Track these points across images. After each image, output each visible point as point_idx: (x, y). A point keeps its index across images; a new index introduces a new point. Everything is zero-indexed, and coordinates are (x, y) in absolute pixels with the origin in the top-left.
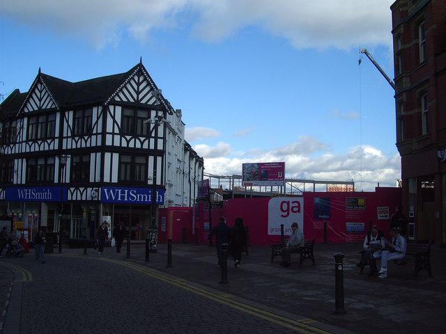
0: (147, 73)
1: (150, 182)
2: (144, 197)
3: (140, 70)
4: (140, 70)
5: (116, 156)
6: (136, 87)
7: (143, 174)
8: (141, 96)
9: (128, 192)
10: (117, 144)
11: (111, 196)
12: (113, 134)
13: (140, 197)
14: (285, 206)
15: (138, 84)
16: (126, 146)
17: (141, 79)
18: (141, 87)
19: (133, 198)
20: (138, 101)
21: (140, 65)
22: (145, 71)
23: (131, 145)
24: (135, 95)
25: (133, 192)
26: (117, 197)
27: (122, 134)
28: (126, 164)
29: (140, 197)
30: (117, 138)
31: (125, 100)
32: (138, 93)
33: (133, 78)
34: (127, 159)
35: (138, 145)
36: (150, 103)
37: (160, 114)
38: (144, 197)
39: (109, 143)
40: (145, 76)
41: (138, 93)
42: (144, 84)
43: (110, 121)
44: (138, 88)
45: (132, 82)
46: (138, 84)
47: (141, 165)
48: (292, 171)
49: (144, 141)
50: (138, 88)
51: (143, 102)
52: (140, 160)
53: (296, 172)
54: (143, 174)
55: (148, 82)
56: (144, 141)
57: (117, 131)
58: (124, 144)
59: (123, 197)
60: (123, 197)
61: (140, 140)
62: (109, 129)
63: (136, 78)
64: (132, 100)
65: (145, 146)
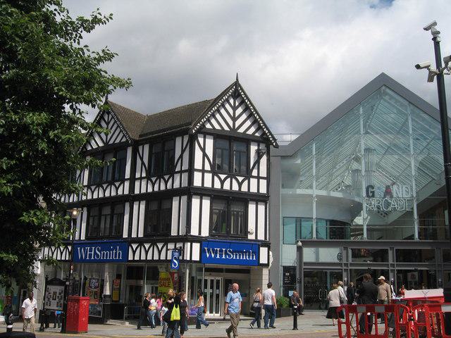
1: (125, 235)
3: (236, 90)
8: (238, 123)
10: (208, 184)
12: (203, 171)
15: (235, 108)
20: (234, 130)
22: (243, 91)
23: (227, 186)
24: (231, 123)
31: (217, 127)
35: (235, 187)
36: (118, 141)
41: (234, 119)
43: (198, 154)
44: (234, 113)
45: (227, 106)
46: (235, 108)
50: (234, 113)
52: (236, 208)
58: (217, 185)
62: (198, 164)
63: (232, 101)
64: (226, 128)
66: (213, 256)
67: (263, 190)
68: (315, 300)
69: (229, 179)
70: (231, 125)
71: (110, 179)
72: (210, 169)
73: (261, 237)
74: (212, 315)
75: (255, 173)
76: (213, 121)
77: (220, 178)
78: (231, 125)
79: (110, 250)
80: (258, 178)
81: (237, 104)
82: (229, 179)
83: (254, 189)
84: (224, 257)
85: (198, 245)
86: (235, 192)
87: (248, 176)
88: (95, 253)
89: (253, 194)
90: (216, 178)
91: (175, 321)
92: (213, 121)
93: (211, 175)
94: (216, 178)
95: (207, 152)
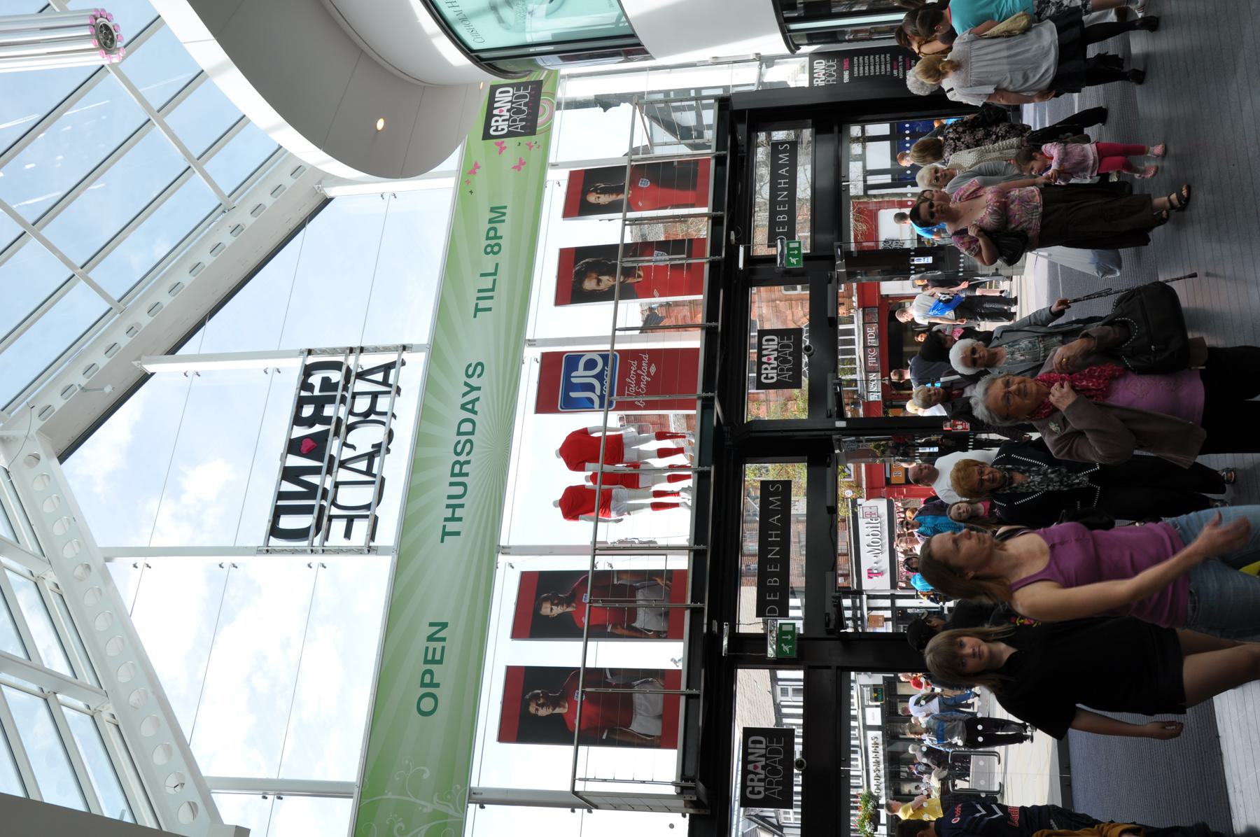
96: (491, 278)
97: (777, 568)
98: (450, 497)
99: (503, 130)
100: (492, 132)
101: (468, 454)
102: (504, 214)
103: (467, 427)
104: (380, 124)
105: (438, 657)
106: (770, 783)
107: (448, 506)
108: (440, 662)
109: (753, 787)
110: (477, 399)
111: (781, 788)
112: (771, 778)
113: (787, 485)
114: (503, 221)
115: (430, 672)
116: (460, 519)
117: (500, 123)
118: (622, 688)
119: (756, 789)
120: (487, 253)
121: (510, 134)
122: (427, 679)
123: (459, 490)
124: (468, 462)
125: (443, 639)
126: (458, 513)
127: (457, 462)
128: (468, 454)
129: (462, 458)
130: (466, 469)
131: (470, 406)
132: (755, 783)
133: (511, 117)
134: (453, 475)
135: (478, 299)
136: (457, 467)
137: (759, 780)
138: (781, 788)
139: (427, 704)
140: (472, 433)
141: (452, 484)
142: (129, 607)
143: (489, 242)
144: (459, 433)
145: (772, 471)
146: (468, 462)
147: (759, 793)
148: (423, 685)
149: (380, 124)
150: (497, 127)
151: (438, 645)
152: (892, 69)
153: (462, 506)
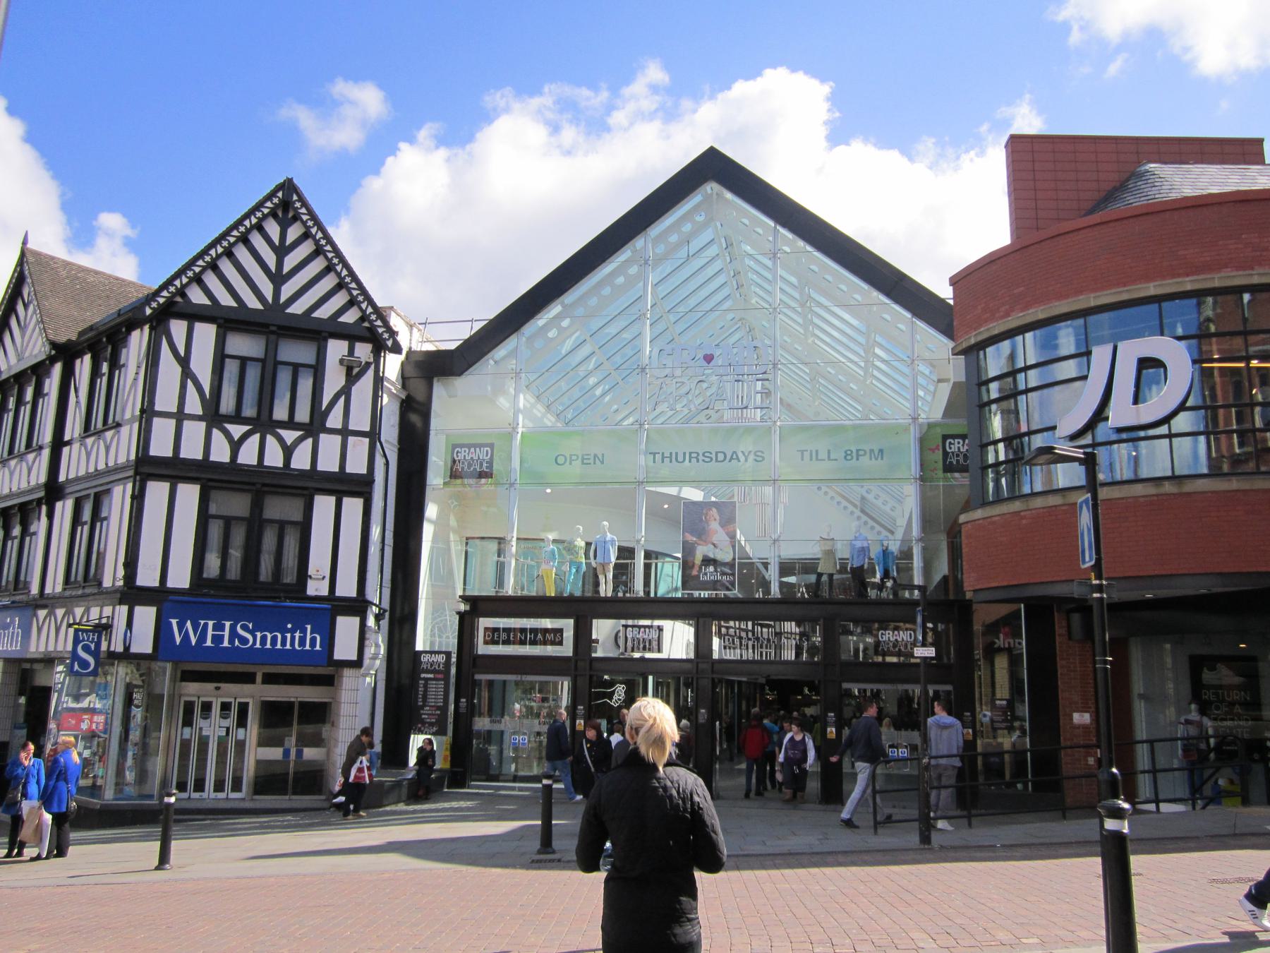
0: (311, 213)
1: (317, 587)
2: (274, 640)
3: (286, 205)
4: (286, 205)
5: (189, 494)
6: (270, 259)
7: (290, 559)
8: (287, 290)
9: (233, 628)
10: (192, 450)
11: (186, 637)
12: (180, 416)
13: (264, 639)
14: (849, 452)
15: (282, 251)
16: (279, 463)
17: (294, 232)
18: (290, 262)
19: (244, 641)
20: (276, 307)
21: (288, 187)
22: (305, 204)
23: (248, 456)
24: (267, 288)
25: (245, 628)
26: (202, 638)
27: (213, 417)
28: (228, 522)
29: (264, 639)
30: (194, 433)
31: (226, 300)
32: (278, 279)
33: (259, 228)
34: (236, 504)
35: (274, 458)
36: (324, 312)
37: (363, 351)
38: (274, 640)
39: (161, 447)
40: (317, 242)
41: (278, 279)
42: (306, 249)
43: (169, 370)
44: (280, 264)
45: (257, 240)
46: (282, 251)
47: (282, 525)
48: (1199, 427)
49: (245, 437)
50: (280, 264)
51: (298, 308)
52: (280, 508)
53: (41, 816)
54: (290, 559)
55: (317, 242)
56: (245, 437)
57: (194, 405)
58: (221, 453)
59: (218, 639)
60: (218, 639)
61: (281, 440)
62: (166, 399)
63: (273, 229)
64: (253, 303)
65: (301, 460)
66: (194, 641)
67: (357, 465)
68: (858, 715)
69: (257, 437)
70: (269, 294)
71: (303, 415)
72: (201, 413)
73: (347, 588)
74: (221, 795)
75: (334, 420)
76: (211, 280)
77: (281, 440)
78: (269, 294)
79: (284, 631)
80: (345, 432)
81: (290, 240)
82: (257, 437)
83: (329, 463)
84: (226, 644)
85: (152, 611)
86: (272, 471)
87: (315, 427)
88: (234, 633)
89: (328, 476)
90: (216, 433)
91: (1087, 761)
92: (211, 280)
93: (202, 426)
94: (216, 433)
95: (194, 366)
96: (826, 456)
97: (559, 631)
98: (677, 454)
99: (950, 448)
100: (948, 441)
101: (703, 460)
102: (876, 459)
103: (721, 457)
104: (666, 506)
105: (585, 461)
106: (958, 456)
107: (671, 454)
108: (583, 463)
109: (953, 444)
110: (739, 461)
111: (955, 463)
112: (961, 456)
113: (560, 643)
114: (871, 459)
115: (577, 459)
116: (663, 462)
117: (957, 445)
118: (290, 705)
119: (952, 446)
120: (846, 452)
121: (945, 454)
122: (574, 458)
123: (680, 459)
124: (698, 461)
125: (595, 463)
126: (667, 460)
127: (698, 454)
128: (703, 460)
129: (701, 458)
130: (694, 460)
131: (734, 457)
132: (957, 445)
133: (962, 453)
134: (690, 453)
135: (811, 451)
136: (695, 455)
137: (959, 448)
138: (955, 463)
139: (561, 460)
140: (717, 461)
141: (684, 454)
142: (460, 343)
143: (854, 451)
144: (717, 453)
145: (569, 635)
146: (698, 461)
147: (950, 448)
148: (571, 455)
149: (666, 506)
150: (953, 444)
151: (592, 461)
152: (430, 706)
153: (671, 461)
